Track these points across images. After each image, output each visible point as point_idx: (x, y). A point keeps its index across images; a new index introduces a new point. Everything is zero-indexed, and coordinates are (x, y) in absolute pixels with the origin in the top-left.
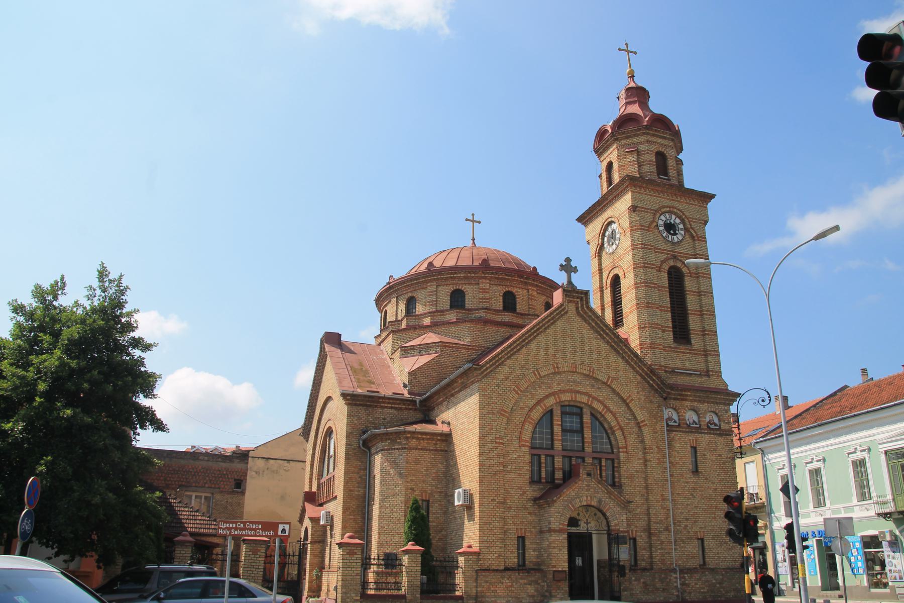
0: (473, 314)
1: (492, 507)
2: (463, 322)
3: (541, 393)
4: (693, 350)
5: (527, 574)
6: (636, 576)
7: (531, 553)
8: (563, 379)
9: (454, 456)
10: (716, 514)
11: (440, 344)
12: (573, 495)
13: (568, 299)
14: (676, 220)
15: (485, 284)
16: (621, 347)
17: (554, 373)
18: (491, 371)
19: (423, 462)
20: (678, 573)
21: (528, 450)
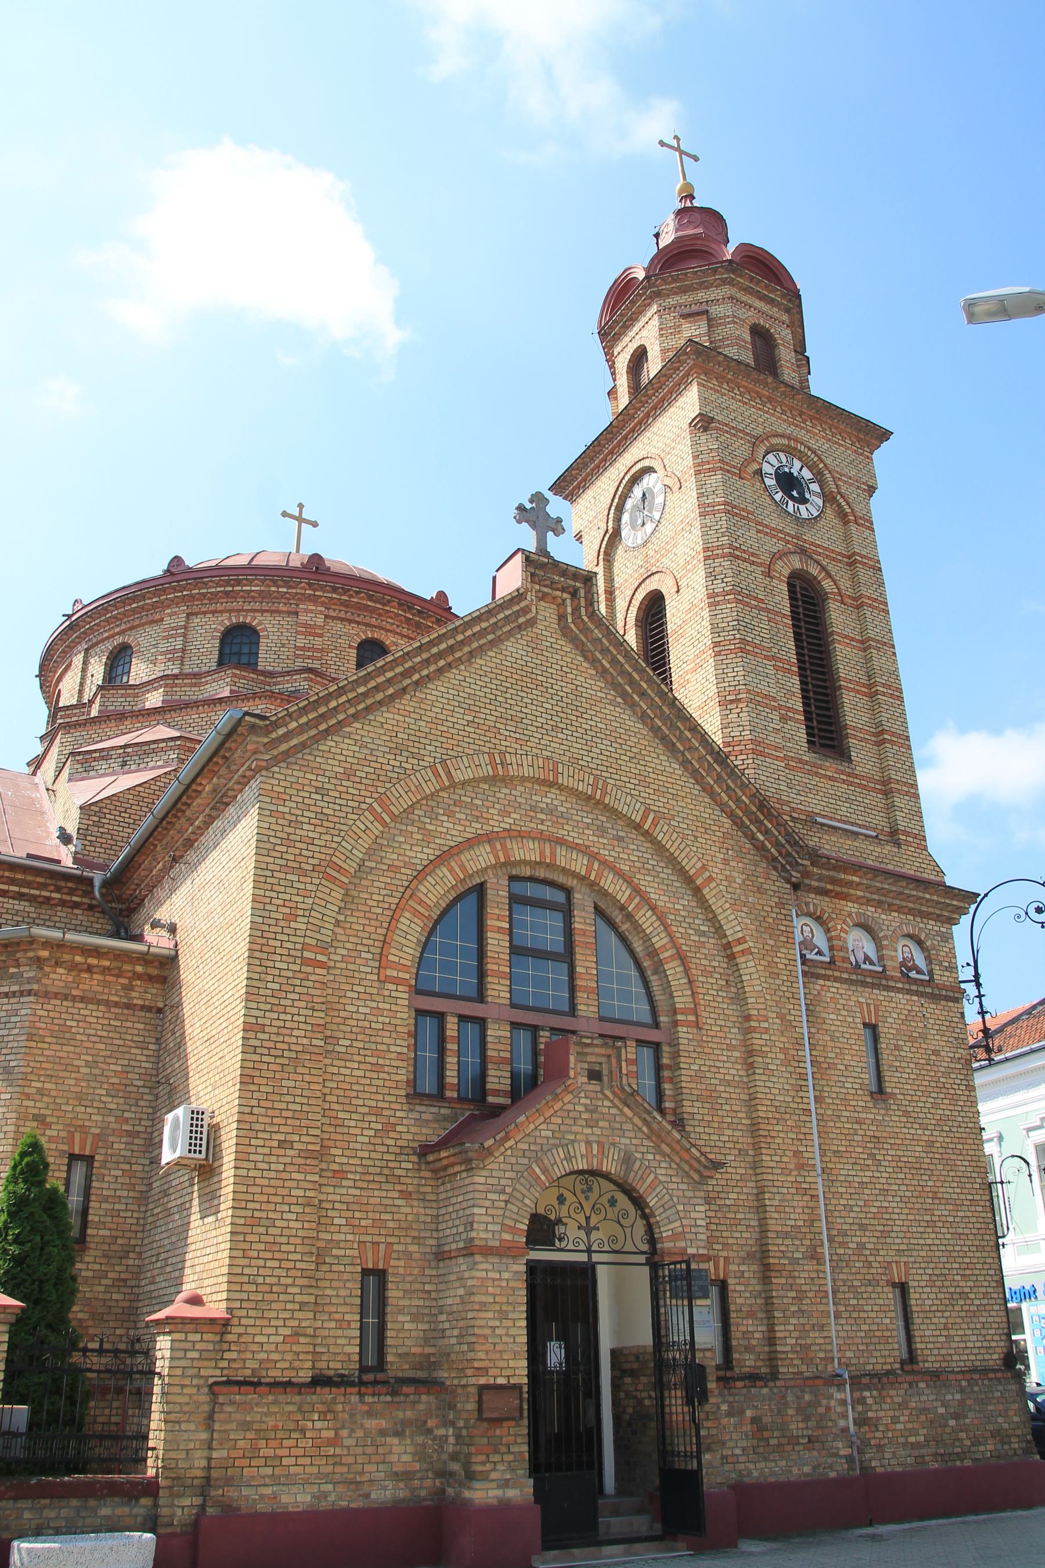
1: (281, 1167)
2: (248, 700)
4: (856, 776)
5: (389, 1398)
6: (731, 1399)
7: (407, 1326)
8: (519, 799)
9: (179, 1021)
10: (936, 1212)
11: (178, 743)
12: (548, 1138)
13: (537, 587)
15: (312, 615)
16: (681, 732)
17: (493, 780)
18: (304, 745)
19: (85, 1038)
20: (848, 1386)
21: (406, 996)
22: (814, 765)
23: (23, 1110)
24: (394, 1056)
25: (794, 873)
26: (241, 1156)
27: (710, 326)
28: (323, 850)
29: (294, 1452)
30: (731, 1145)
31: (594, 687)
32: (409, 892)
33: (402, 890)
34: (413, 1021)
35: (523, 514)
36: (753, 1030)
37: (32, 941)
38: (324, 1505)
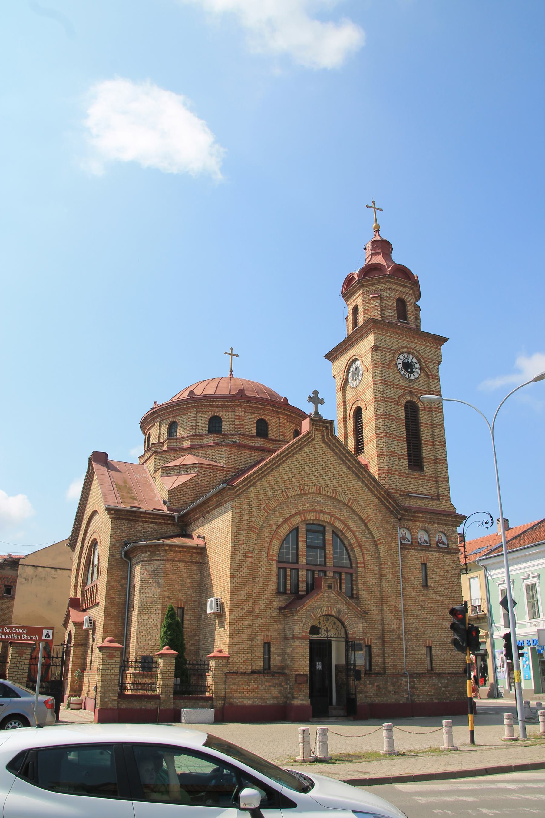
0: (228, 438)
1: (242, 615)
3: (288, 512)
4: (425, 476)
5: (271, 677)
7: (276, 658)
9: (208, 568)
11: (198, 465)
12: (315, 606)
13: (315, 427)
14: (411, 359)
15: (240, 412)
16: (362, 472)
18: (244, 491)
22: (410, 474)
23: (164, 595)
24: (272, 582)
25: (399, 516)
26: (231, 613)
27: (381, 301)
28: (251, 523)
29: (247, 690)
30: (374, 604)
31: (333, 459)
32: (275, 532)
33: (273, 532)
34: (277, 571)
35: (310, 399)
36: (383, 568)
37: (163, 545)
38: (255, 704)
